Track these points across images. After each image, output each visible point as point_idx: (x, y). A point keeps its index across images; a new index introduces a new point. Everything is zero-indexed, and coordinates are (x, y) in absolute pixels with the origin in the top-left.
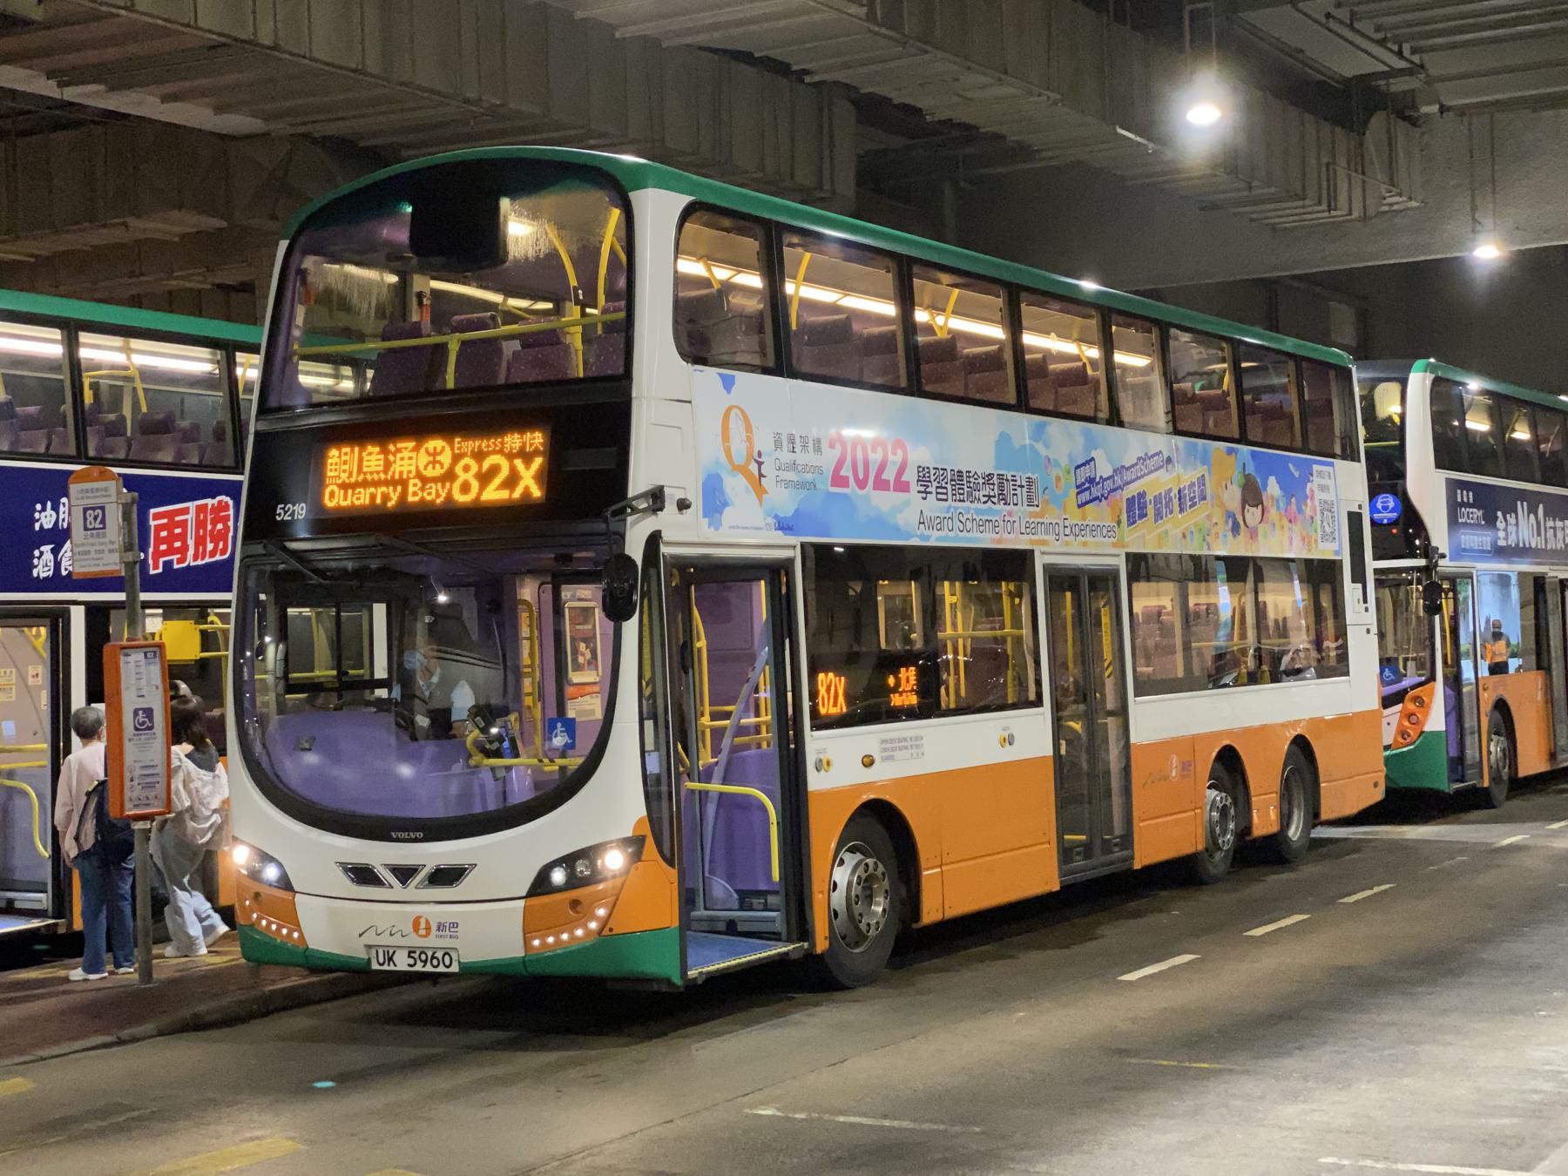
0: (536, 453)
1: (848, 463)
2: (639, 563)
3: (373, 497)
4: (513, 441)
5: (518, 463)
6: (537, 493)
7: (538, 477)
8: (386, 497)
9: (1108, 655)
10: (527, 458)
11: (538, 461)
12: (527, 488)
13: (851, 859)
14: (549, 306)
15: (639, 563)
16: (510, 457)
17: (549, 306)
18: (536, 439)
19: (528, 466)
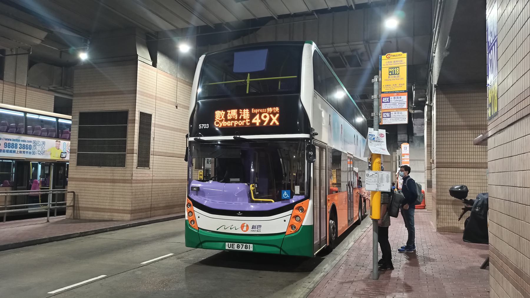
0: (277, 113)
1: (500, 66)
2: (400, 213)
3: (233, 124)
4: (270, 110)
5: (271, 115)
6: (278, 123)
7: (278, 119)
8: (233, 124)
9: (36, 117)
10: (274, 115)
11: (277, 115)
12: (274, 123)
13: (363, 286)
14: (312, 164)
15: (400, 213)
16: (269, 114)
17: (312, 164)
18: (277, 109)
19: (274, 116)
